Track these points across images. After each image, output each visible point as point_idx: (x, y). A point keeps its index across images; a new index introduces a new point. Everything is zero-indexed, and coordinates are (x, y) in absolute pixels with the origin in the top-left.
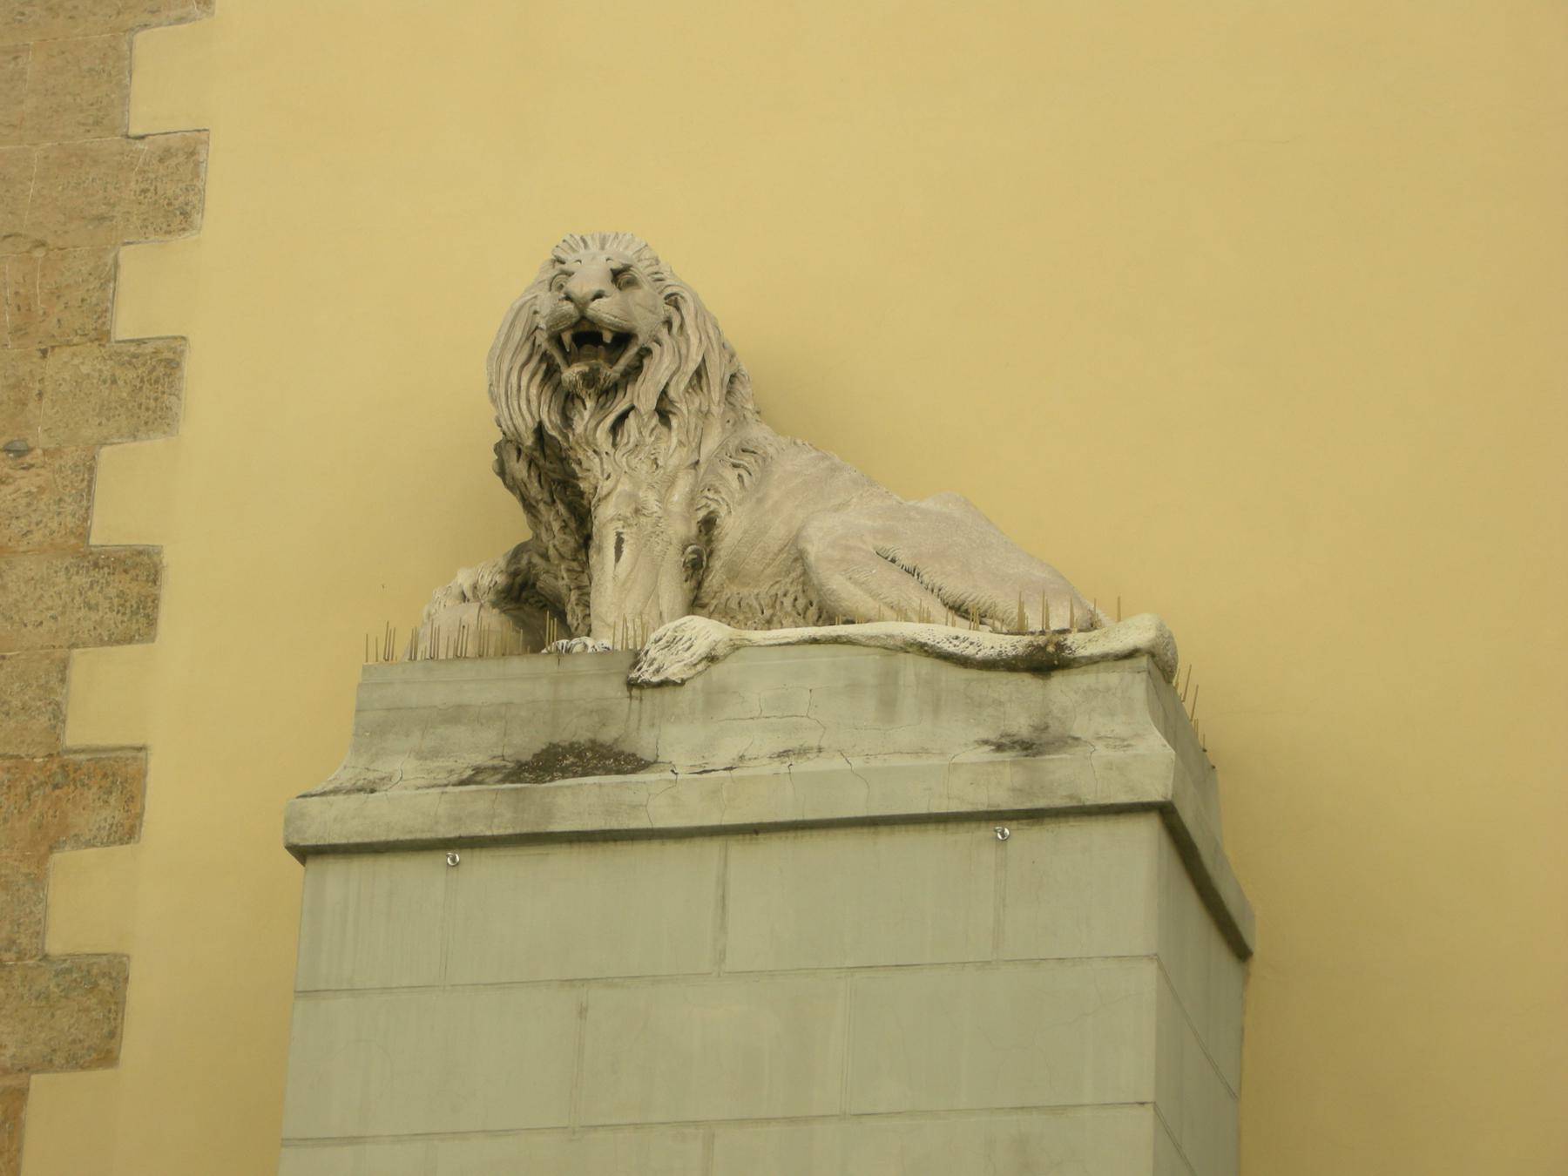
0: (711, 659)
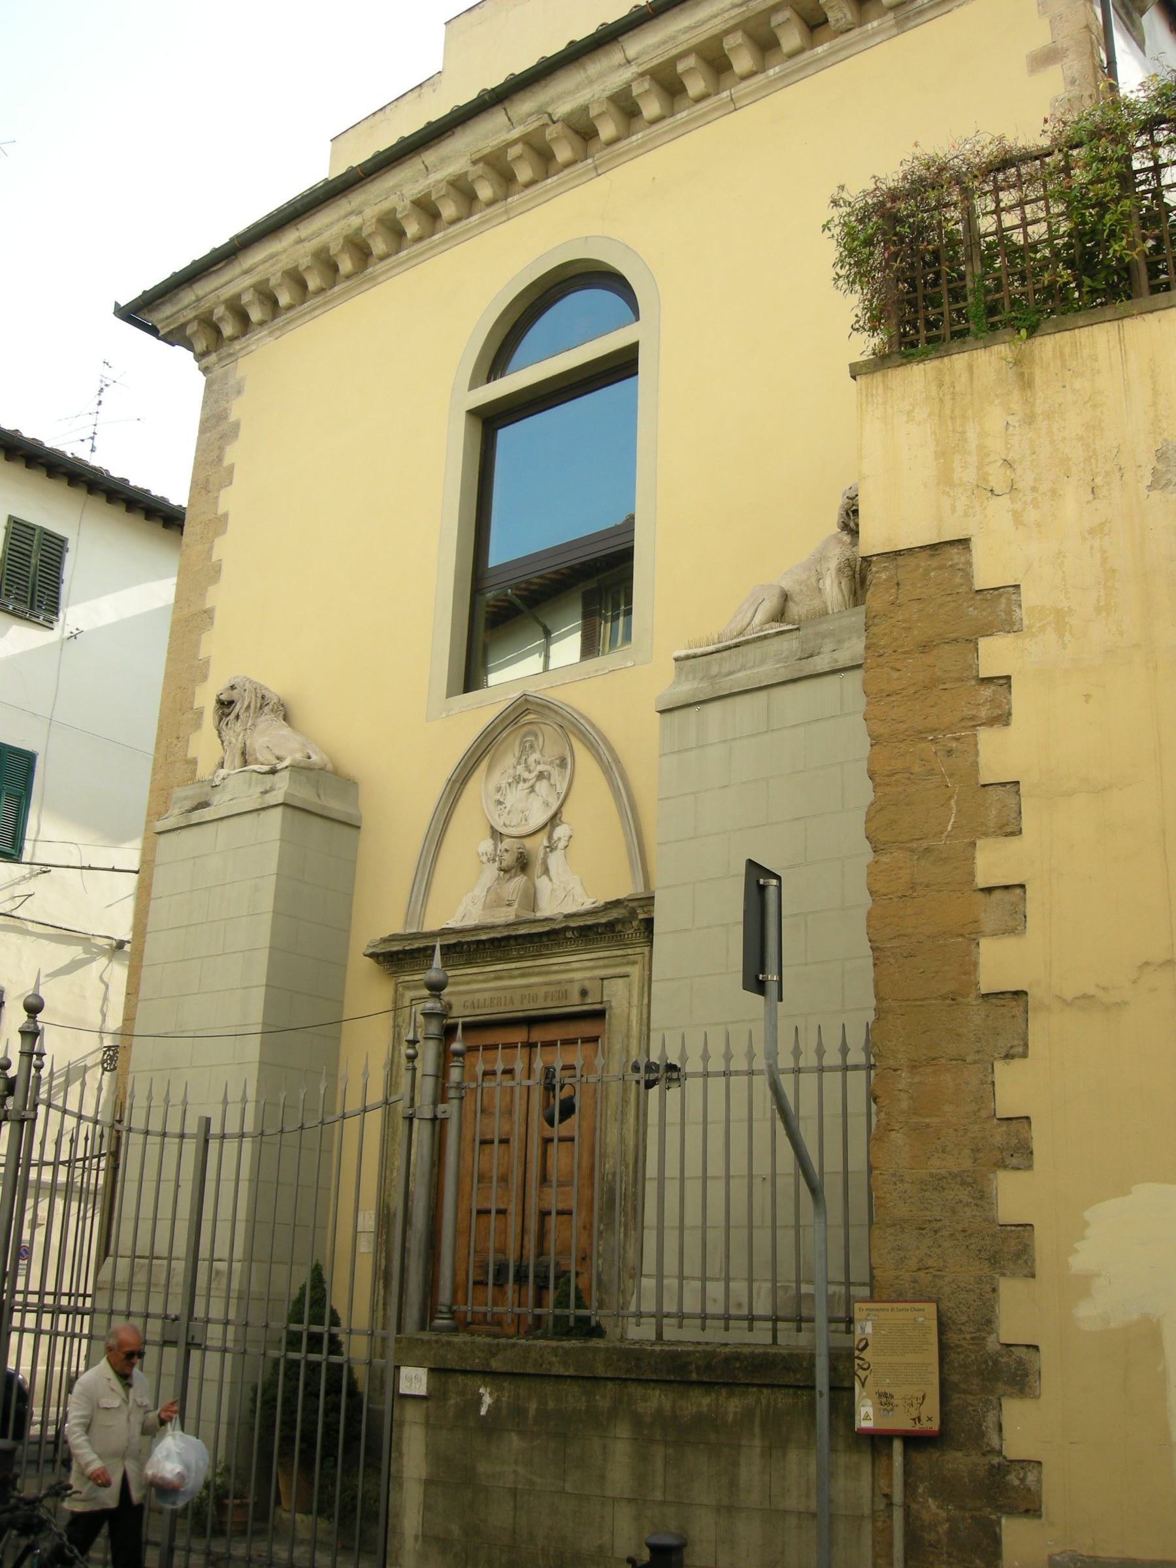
0: (224, 779)
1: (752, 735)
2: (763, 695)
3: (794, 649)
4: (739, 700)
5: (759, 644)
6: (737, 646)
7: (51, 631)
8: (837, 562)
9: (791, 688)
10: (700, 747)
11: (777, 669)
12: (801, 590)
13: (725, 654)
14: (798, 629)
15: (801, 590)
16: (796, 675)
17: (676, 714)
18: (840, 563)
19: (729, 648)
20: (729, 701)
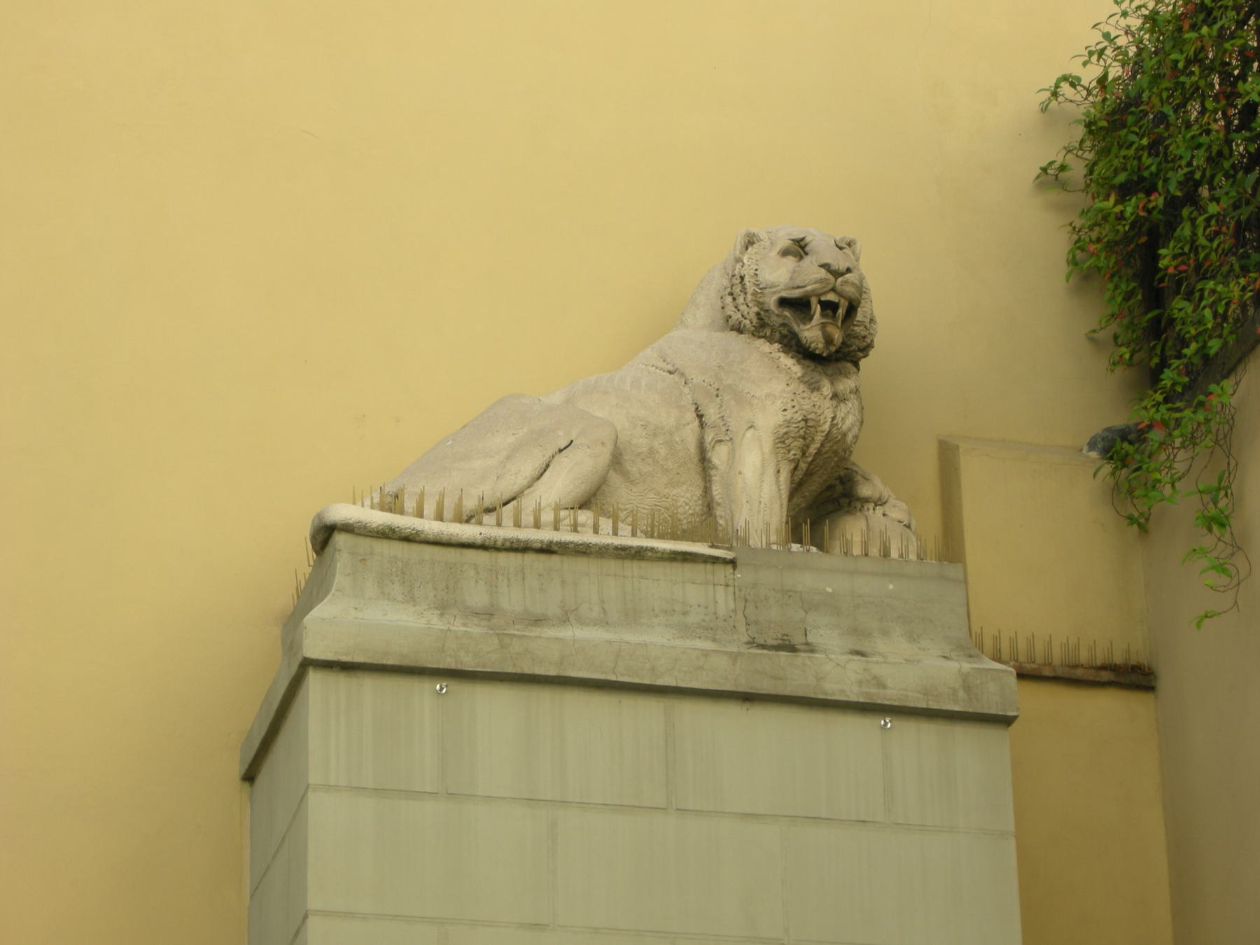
1: (620, 808)
2: (650, 710)
3: (722, 611)
4: (574, 700)
5: (612, 565)
6: (547, 550)
7: (236, 769)
8: (780, 418)
9: (734, 711)
10: (451, 795)
11: (706, 654)
12: (652, 452)
13: (504, 559)
14: (733, 563)
15: (652, 452)
16: (766, 687)
17: (369, 685)
18: (788, 423)
19: (522, 548)
20: (544, 698)
